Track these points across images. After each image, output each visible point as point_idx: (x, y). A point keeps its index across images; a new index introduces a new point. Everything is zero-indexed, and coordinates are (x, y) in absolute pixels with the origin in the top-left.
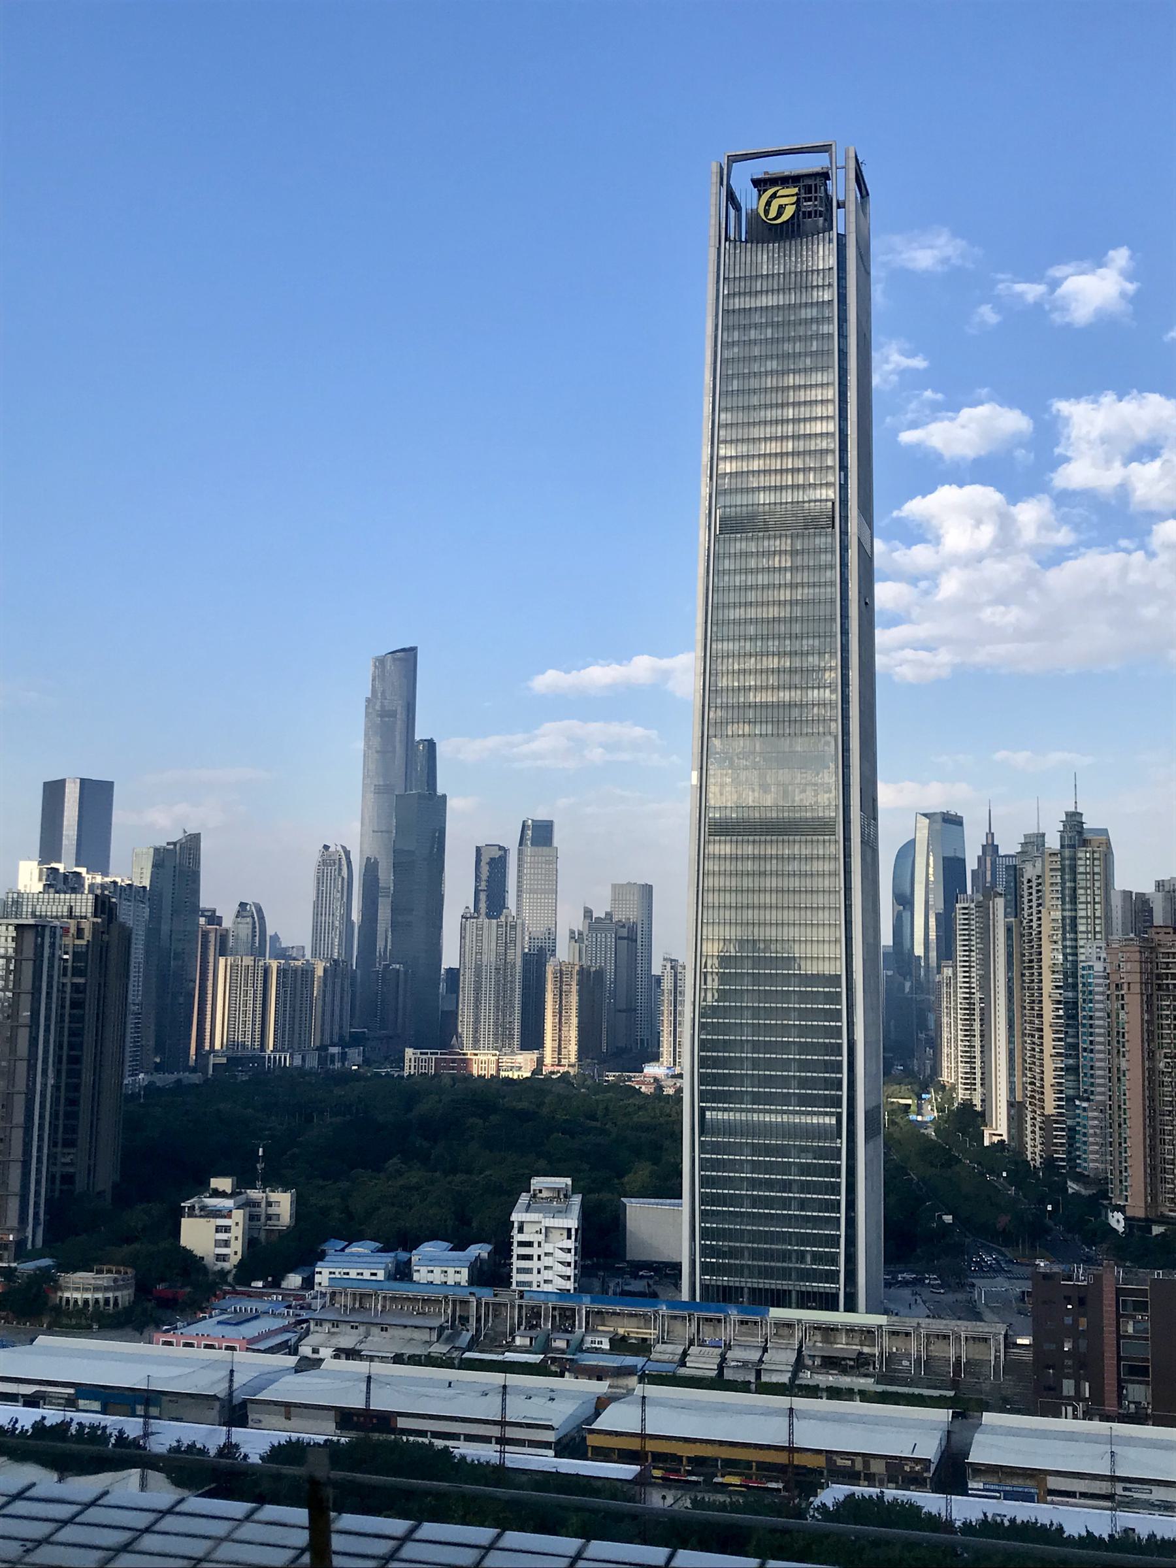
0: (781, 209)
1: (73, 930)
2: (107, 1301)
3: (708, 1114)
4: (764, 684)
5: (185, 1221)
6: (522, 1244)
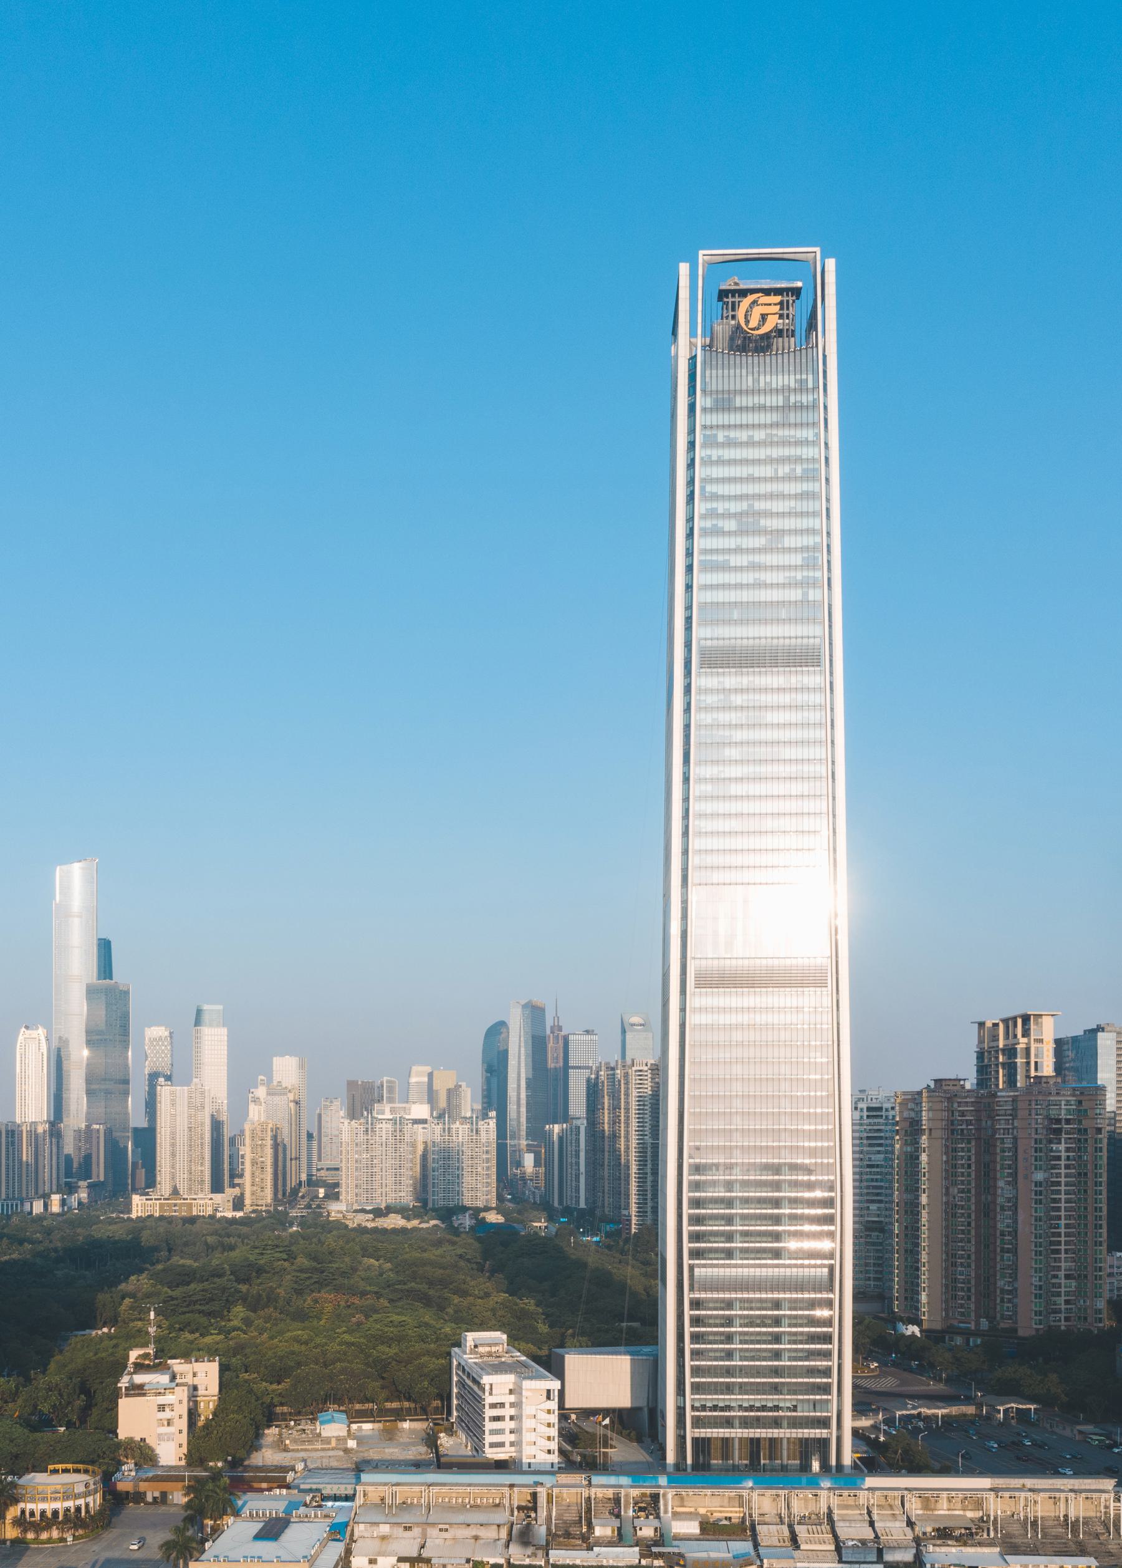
0: (764, 317)
1: (1033, 1103)
2: (78, 1509)
5: (124, 1404)
6: (493, 1406)
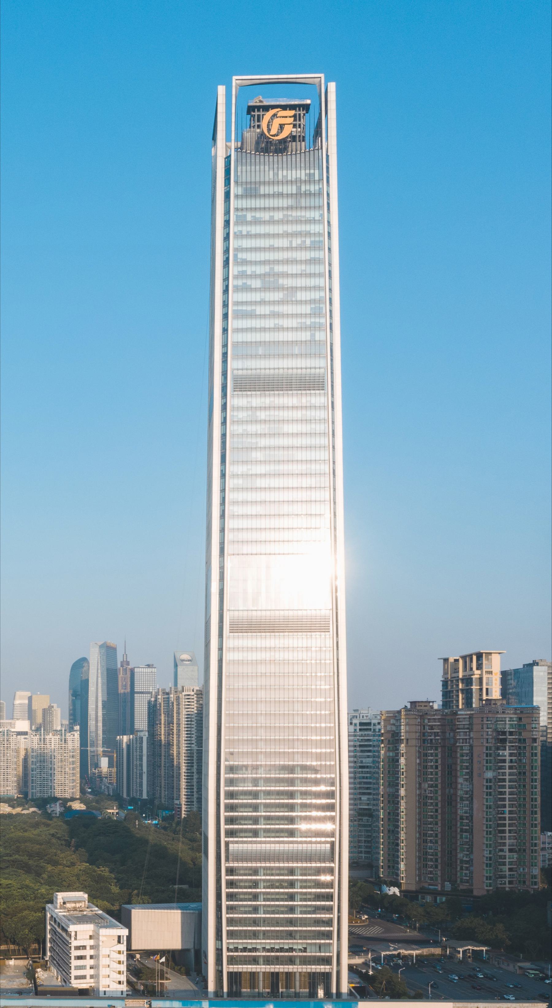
0: (282, 127)
3: (231, 846)
4: (262, 180)
6: (78, 948)
